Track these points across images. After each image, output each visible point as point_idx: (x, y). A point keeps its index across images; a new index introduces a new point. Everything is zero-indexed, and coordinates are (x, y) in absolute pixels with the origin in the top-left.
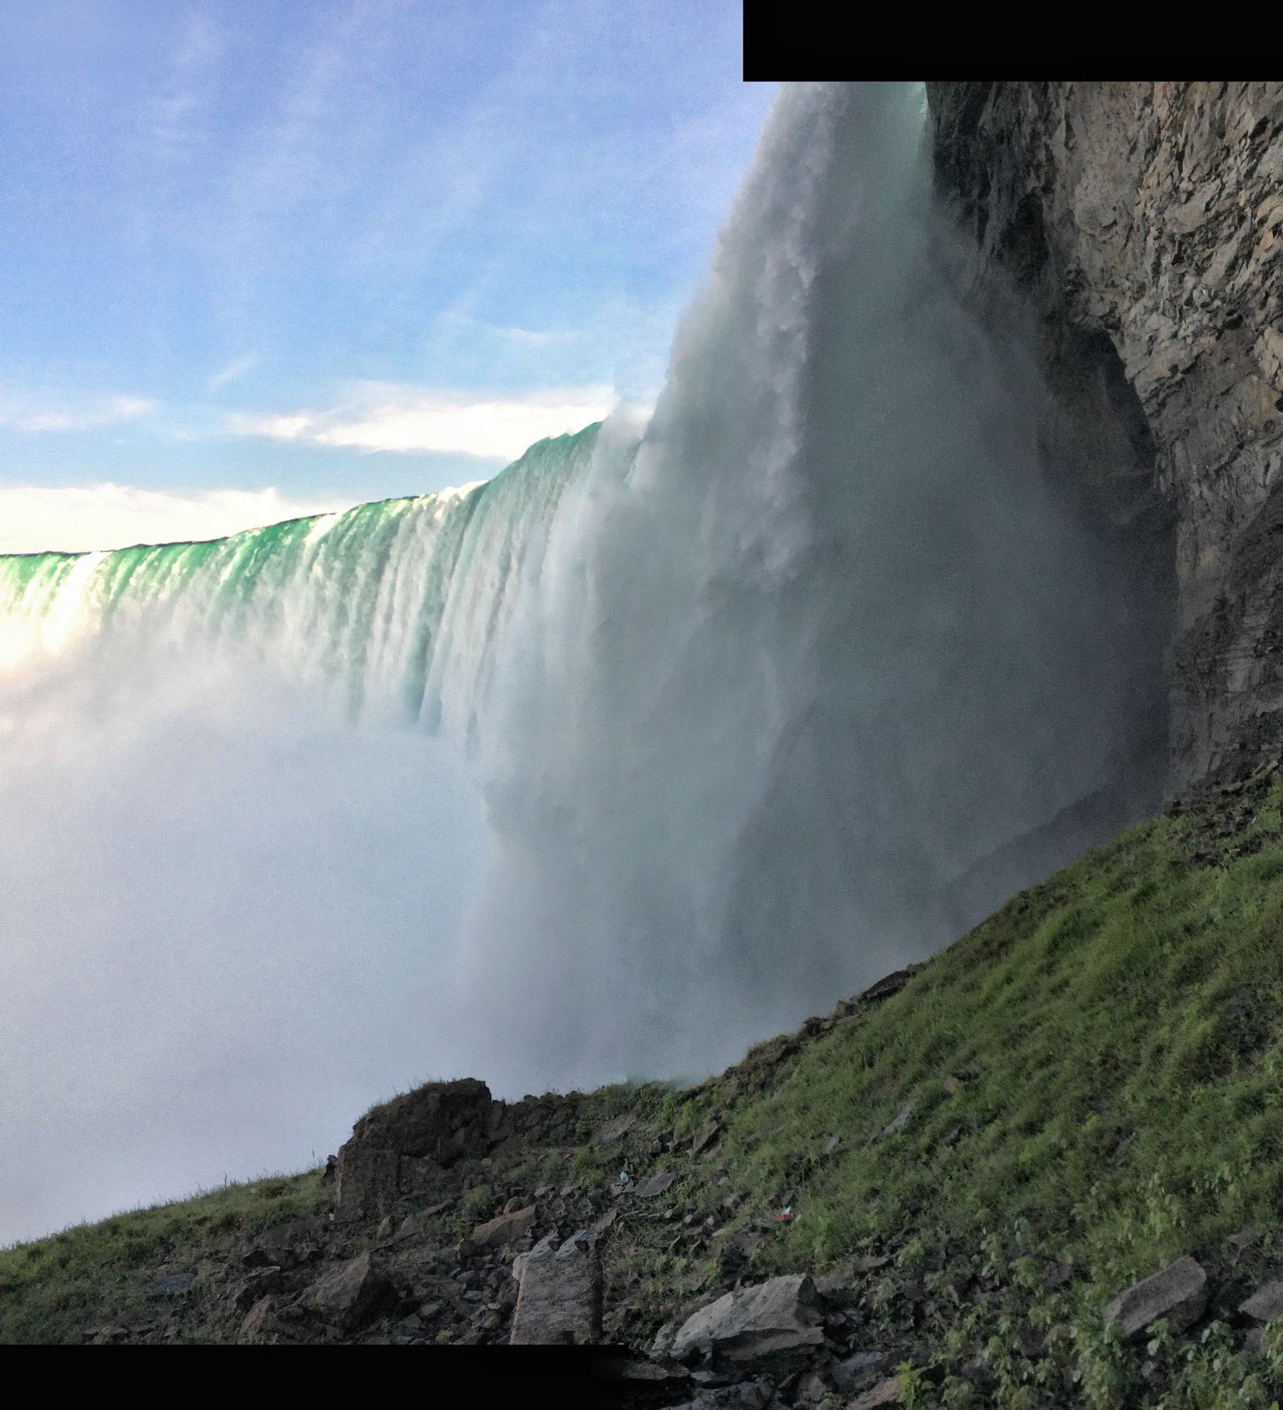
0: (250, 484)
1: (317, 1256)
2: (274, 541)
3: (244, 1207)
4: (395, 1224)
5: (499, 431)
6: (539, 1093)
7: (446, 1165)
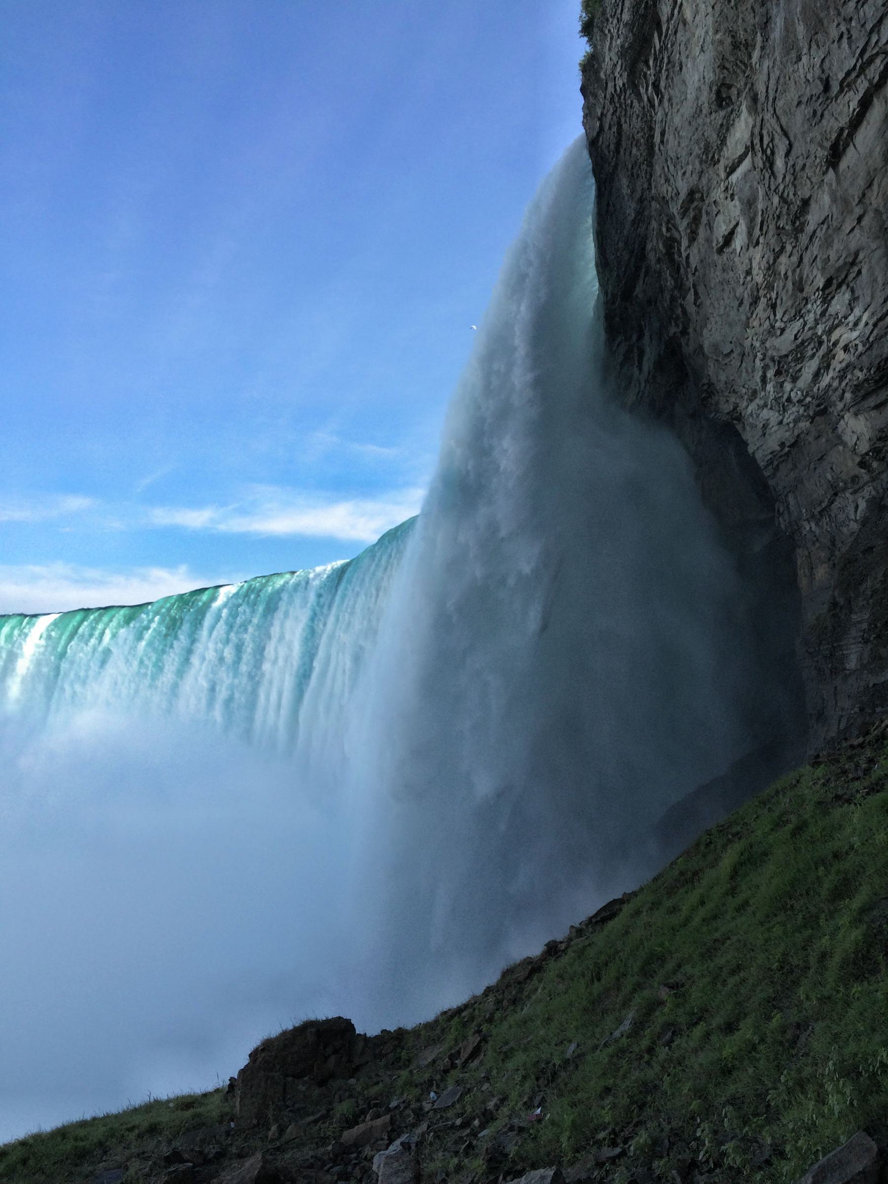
0: (170, 564)
1: (221, 1155)
2: (188, 610)
3: (164, 1118)
4: (281, 1131)
5: (357, 523)
6: (392, 1028)
7: (322, 1083)
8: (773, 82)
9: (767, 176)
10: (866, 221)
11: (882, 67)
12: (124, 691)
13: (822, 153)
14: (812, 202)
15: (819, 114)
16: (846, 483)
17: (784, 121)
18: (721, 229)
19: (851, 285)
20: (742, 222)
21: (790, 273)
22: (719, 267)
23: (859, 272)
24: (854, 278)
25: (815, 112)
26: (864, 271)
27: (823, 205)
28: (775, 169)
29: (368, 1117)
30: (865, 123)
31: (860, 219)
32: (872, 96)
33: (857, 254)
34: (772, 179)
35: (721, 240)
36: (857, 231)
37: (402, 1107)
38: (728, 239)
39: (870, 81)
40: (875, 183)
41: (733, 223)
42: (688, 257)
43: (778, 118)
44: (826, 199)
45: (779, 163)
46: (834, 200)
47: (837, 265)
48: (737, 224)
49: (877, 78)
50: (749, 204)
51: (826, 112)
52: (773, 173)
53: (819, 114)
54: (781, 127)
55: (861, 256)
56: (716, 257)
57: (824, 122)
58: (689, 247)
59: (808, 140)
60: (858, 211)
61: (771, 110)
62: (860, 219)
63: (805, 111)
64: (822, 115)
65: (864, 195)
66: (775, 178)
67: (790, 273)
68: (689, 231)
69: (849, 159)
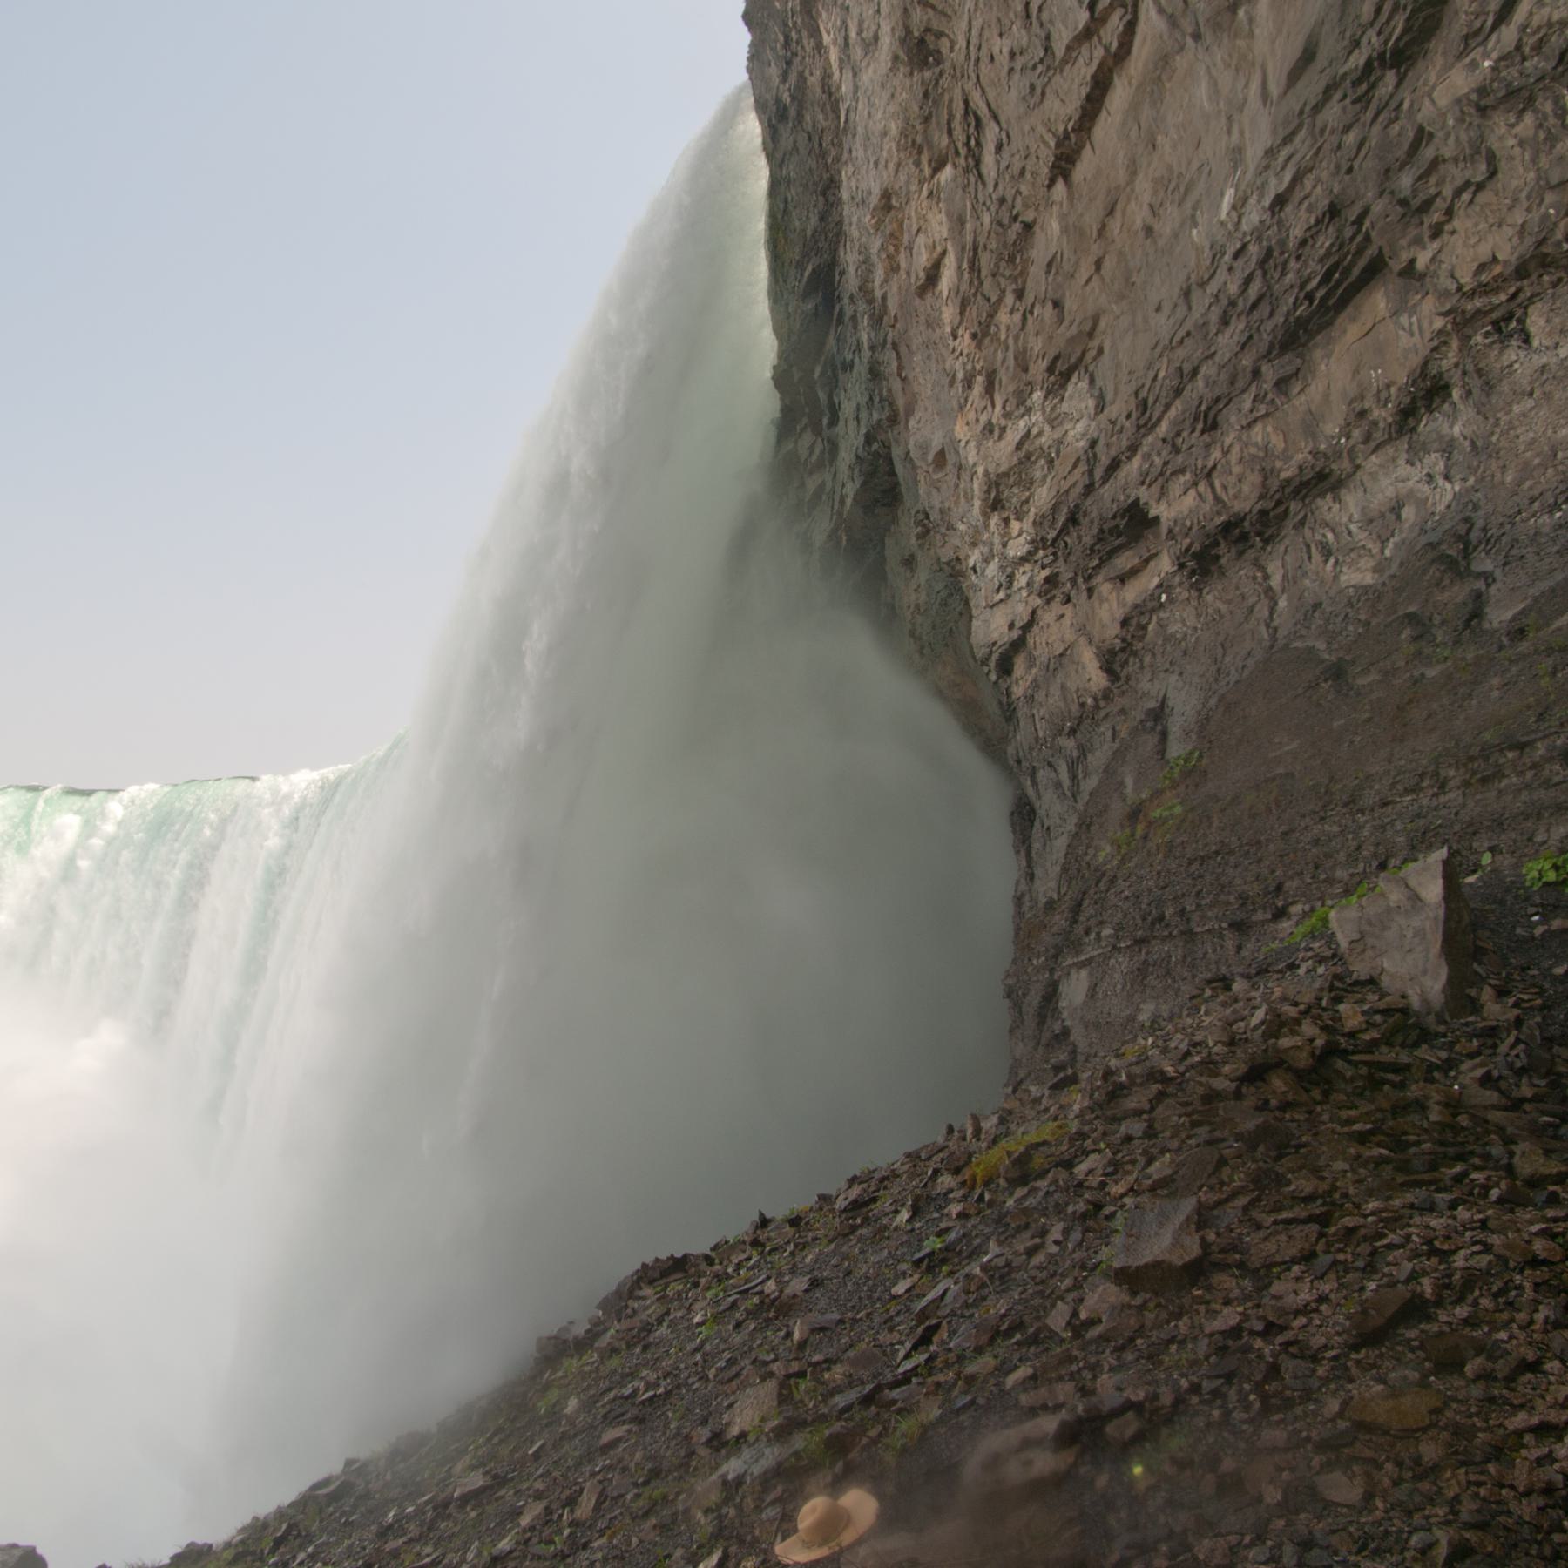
8: (975, 32)
9: (972, 179)
10: (1107, 265)
11: (1121, 28)
12: (1285, 1042)
13: (1047, 155)
14: (1037, 229)
15: (1038, 90)
16: (1095, 699)
17: (991, 94)
18: (923, 259)
19: (1091, 368)
20: (950, 249)
21: (1011, 341)
22: (922, 319)
23: (1100, 351)
24: (1095, 359)
25: (1032, 87)
26: (1106, 350)
27: (1050, 235)
28: (984, 170)
29: (1292, 1187)
30: (1104, 112)
31: (1098, 264)
32: (1111, 71)
33: (1096, 320)
34: (980, 187)
35: (922, 275)
36: (1095, 282)
37: (413, 1529)
38: (932, 276)
39: (1107, 49)
40: (1119, 206)
41: (939, 249)
42: (884, 298)
43: (983, 92)
44: (1055, 226)
45: (989, 159)
46: (1065, 230)
47: (1069, 334)
48: (944, 253)
49: (1115, 45)
50: (958, 222)
51: (1048, 90)
52: (980, 176)
53: (1038, 90)
54: (989, 105)
55: (1102, 324)
56: (917, 301)
57: (1047, 103)
58: (886, 281)
59: (1027, 128)
60: (1096, 249)
61: (973, 76)
62: (1098, 264)
63: (1019, 83)
64: (1043, 94)
65: (1104, 226)
66: (984, 184)
67: (1011, 341)
68: (884, 256)
69: (1084, 169)
